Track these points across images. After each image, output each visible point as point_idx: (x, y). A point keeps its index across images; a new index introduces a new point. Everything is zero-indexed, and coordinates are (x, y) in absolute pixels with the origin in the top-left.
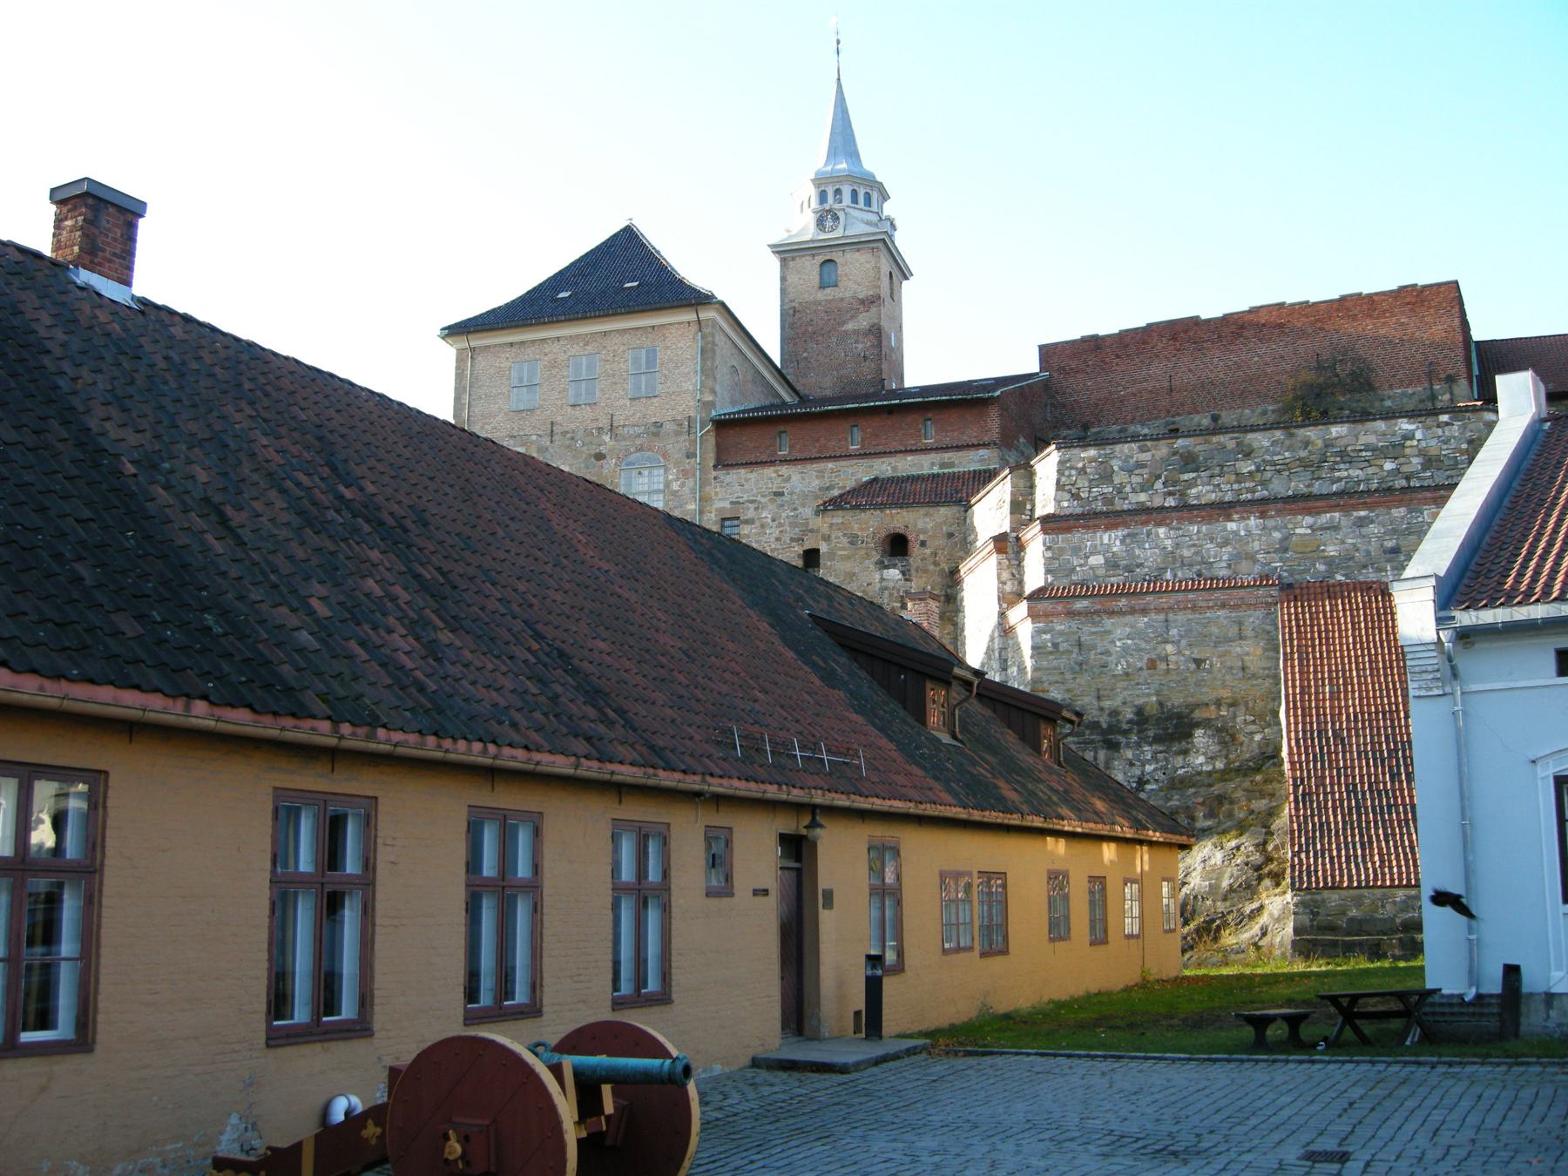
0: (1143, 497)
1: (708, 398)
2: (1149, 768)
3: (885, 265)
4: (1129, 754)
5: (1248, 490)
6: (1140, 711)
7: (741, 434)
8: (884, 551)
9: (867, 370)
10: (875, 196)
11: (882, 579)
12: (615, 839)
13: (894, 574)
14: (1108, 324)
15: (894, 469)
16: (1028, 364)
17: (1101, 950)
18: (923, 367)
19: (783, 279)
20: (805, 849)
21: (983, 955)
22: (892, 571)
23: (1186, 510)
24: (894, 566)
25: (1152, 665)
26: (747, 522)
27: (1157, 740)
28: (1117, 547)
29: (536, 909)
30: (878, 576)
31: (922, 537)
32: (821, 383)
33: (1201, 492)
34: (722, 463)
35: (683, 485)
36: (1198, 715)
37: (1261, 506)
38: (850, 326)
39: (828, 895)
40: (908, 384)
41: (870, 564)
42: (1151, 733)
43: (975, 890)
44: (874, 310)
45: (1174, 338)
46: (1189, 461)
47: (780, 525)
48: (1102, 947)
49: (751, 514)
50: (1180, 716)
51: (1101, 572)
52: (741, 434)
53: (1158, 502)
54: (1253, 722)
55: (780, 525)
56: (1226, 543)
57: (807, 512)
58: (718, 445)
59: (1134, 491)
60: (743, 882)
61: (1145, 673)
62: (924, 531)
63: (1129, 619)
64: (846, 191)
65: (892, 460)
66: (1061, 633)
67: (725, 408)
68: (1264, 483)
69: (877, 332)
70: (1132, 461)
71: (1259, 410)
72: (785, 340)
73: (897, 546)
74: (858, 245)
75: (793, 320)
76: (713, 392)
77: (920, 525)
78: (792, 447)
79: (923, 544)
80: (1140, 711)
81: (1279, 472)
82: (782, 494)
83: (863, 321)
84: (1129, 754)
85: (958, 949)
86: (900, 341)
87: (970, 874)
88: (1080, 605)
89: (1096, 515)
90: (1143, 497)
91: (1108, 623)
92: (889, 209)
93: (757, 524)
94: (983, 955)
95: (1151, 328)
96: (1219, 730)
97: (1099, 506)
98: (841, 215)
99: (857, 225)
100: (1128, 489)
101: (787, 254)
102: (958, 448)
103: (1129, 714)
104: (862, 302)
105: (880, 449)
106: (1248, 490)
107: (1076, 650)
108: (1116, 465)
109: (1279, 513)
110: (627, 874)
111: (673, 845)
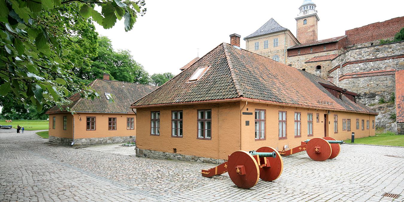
0: (368, 57)
1: (286, 46)
2: (366, 102)
3: (315, 19)
4: (363, 100)
5: (390, 54)
6: (365, 93)
7: (291, 51)
8: (316, 69)
9: (312, 38)
10: (314, 7)
11: (316, 73)
12: (172, 113)
13: (318, 72)
14: (359, 25)
15: (318, 55)
16: (343, 34)
17: (336, 134)
18: (323, 36)
19: (297, 24)
20: (326, 116)
21: (348, 131)
22: (318, 72)
23: (377, 59)
24: (318, 71)
25: (368, 85)
26: (293, 65)
27: (368, 98)
28: (362, 66)
29: (265, 124)
30: (315, 73)
31: (323, 66)
32: (303, 42)
33: (380, 55)
34: (289, 56)
35: (282, 60)
36: (377, 93)
37: (393, 57)
38: (309, 31)
39: (329, 122)
40: (318, 40)
41: (314, 71)
42: (367, 96)
43: (347, 122)
44: (313, 27)
45: (374, 26)
46: (378, 50)
47: (298, 65)
48: (285, 140)
49: (294, 64)
50: (373, 94)
51: (359, 70)
52: (291, 51)
53: (371, 58)
54: (388, 94)
55: (298, 65)
56: (385, 64)
57: (303, 63)
58: (288, 53)
59: (366, 56)
60: (320, 121)
61: (367, 87)
62: (324, 65)
63: (364, 78)
64: (309, 7)
65: (318, 53)
66: (350, 81)
67: (289, 47)
68: (394, 53)
69: (314, 31)
70: (366, 51)
71: (391, 38)
72: (297, 34)
73: (319, 67)
74: (310, 16)
75: (298, 30)
76: (287, 45)
77: (323, 64)
78: (300, 53)
79: (324, 67)
80: (365, 93)
81: (397, 50)
82: (299, 60)
83: (311, 30)
84: (363, 100)
85: (345, 130)
86: (317, 32)
87: (346, 119)
88: (354, 76)
89: (358, 61)
90: (368, 57)
91: (360, 79)
92: (316, 9)
93: (295, 65)
94: (348, 131)
95: (369, 25)
96: (381, 96)
97: (359, 59)
98: (308, 11)
99: (311, 12)
100: (365, 56)
101: (297, 19)
102: (330, 51)
103: (363, 93)
104: (311, 26)
105: (316, 52)
106: (390, 54)
107: (353, 83)
108: (362, 52)
109: (396, 58)
110: (280, 119)
111: (313, 116)
